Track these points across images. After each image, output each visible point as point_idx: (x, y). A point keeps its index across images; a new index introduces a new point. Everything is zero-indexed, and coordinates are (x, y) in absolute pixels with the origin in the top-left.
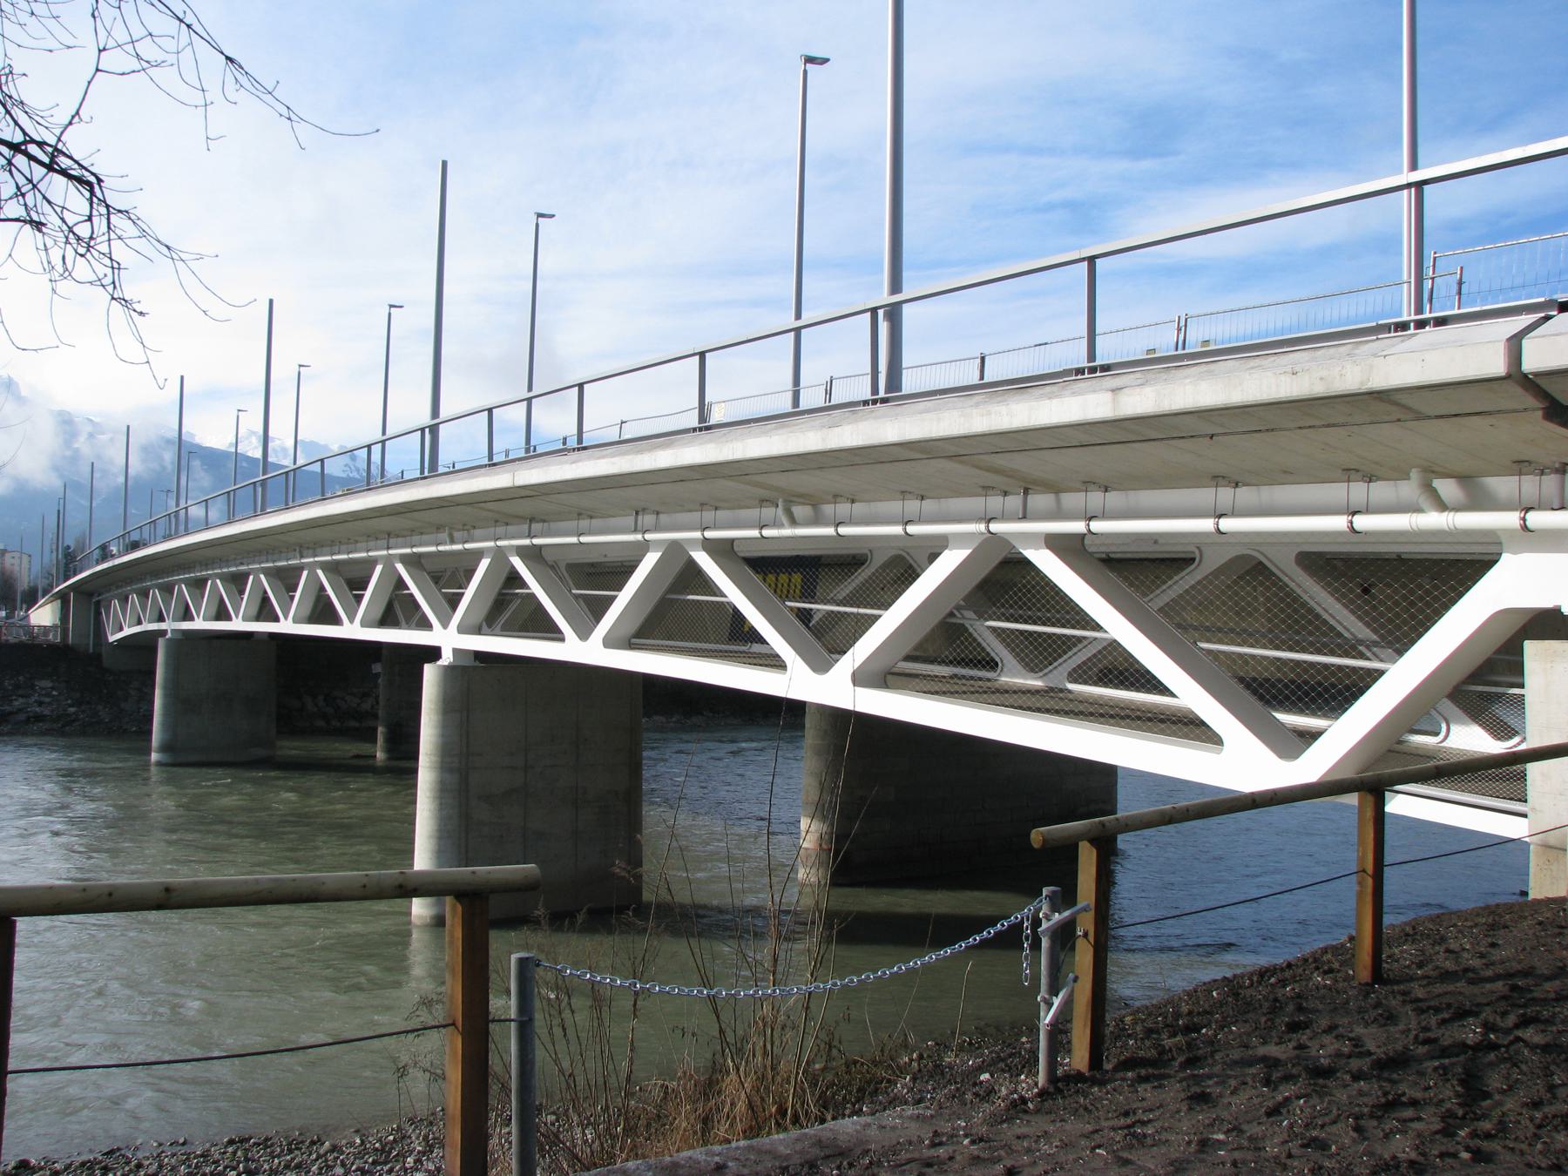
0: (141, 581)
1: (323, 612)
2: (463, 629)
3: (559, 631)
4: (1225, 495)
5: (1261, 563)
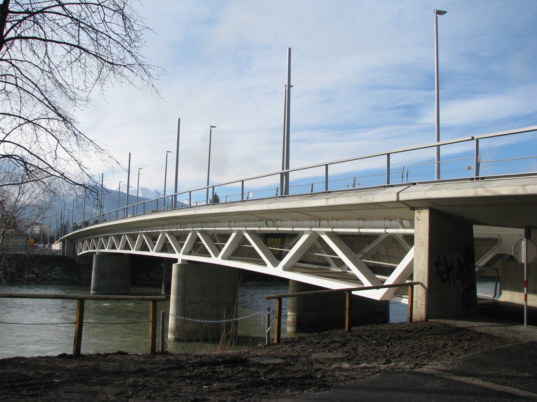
0: (89, 236)
1: (144, 248)
2: (184, 254)
3: (209, 253)
4: (361, 223)
5: (395, 239)
